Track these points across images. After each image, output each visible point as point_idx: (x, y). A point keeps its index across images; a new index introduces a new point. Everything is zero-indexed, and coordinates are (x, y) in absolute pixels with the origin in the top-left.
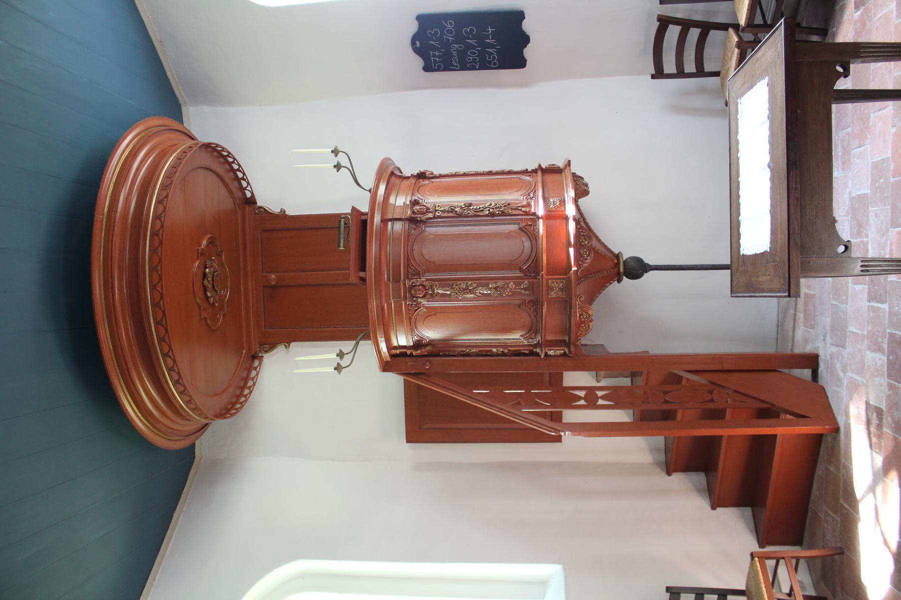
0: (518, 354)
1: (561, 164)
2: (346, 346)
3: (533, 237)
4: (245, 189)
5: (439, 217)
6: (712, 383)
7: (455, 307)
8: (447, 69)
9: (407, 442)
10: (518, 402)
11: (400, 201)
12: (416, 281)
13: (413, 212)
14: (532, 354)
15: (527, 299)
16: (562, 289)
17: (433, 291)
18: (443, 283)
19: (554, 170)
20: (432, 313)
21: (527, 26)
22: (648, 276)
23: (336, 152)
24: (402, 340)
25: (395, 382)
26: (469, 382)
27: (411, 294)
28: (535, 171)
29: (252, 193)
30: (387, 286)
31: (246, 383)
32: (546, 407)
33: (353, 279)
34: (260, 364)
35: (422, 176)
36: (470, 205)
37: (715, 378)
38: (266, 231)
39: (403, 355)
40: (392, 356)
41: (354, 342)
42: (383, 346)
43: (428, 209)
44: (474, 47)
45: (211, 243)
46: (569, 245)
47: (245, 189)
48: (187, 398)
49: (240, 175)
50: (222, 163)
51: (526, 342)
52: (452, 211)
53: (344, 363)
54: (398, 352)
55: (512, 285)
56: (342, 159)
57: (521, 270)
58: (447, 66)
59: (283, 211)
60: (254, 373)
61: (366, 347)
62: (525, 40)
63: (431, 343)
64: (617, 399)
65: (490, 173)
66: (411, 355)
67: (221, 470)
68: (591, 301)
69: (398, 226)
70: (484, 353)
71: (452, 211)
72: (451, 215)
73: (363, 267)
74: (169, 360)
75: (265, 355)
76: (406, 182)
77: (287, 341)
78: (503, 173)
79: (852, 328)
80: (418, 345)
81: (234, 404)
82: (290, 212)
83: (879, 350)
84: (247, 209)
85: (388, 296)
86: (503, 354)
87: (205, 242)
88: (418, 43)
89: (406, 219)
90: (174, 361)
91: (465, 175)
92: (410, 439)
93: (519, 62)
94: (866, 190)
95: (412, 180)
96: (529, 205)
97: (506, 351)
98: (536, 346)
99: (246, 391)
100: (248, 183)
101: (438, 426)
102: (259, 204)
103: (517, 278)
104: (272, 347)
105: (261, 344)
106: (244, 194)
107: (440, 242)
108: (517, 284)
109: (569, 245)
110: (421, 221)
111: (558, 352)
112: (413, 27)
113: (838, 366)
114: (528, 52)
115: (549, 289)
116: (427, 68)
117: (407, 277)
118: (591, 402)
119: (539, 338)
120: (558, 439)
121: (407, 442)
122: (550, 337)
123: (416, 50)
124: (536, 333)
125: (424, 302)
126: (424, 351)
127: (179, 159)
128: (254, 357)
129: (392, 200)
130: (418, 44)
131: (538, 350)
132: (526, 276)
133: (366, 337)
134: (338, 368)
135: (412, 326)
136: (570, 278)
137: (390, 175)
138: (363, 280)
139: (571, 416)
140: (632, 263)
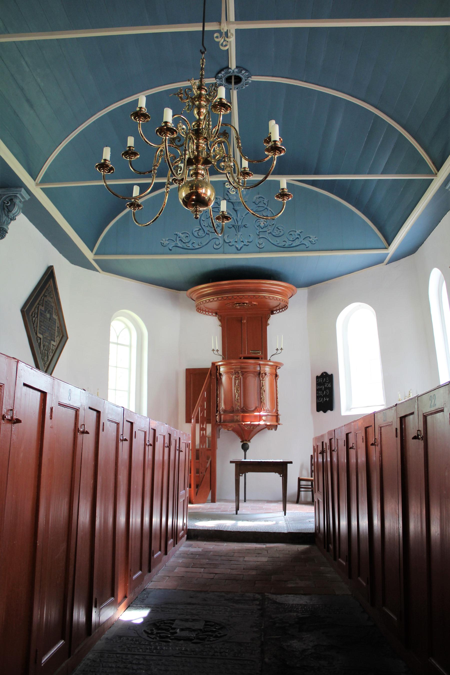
0: (217, 406)
1: (280, 422)
2: (220, 352)
3: (254, 411)
8: (317, 384)
9: (186, 369)
11: (267, 369)
12: (241, 374)
15: (234, 409)
16: (237, 420)
19: (277, 420)
20: (231, 379)
21: (329, 412)
23: (281, 349)
24: (222, 369)
25: (209, 366)
27: (236, 373)
28: (277, 413)
30: (239, 365)
33: (241, 355)
35: (276, 376)
37: (209, 469)
38: (262, 318)
39: (217, 370)
40: (217, 366)
41: (221, 354)
42: (220, 363)
44: (323, 393)
45: (255, 305)
46: (251, 422)
48: (204, 302)
49: (281, 310)
52: (263, 386)
53: (215, 352)
55: (239, 404)
57: (243, 407)
58: (318, 384)
60: (210, 314)
61: (220, 358)
63: (221, 379)
64: (203, 438)
65: (277, 398)
66: (217, 372)
69: (259, 369)
71: (263, 386)
73: (245, 358)
76: (274, 370)
77: (223, 326)
78: (277, 403)
80: (220, 374)
81: (200, 309)
82: (268, 327)
84: (270, 312)
85: (236, 365)
86: (217, 402)
87: (255, 303)
89: (260, 371)
90: (216, 301)
91: (276, 390)
92: (187, 369)
93: (318, 410)
95: (275, 373)
96: (264, 410)
98: (220, 412)
101: (192, 379)
102: (271, 316)
104: (220, 320)
105: (221, 316)
107: (252, 381)
109: (251, 422)
112: (329, 373)
114: (321, 412)
115: (237, 416)
116: (317, 377)
117: (242, 372)
118: (202, 429)
119: (222, 413)
120: (188, 420)
121: (186, 369)
122: (222, 416)
123: (322, 374)
124: (224, 412)
125: (234, 377)
128: (216, 313)
132: (241, 409)
133: (223, 359)
134: (213, 350)
135: (227, 373)
136: (240, 422)
137: (276, 366)
138: (241, 358)
139: (198, 426)
140: (247, 446)
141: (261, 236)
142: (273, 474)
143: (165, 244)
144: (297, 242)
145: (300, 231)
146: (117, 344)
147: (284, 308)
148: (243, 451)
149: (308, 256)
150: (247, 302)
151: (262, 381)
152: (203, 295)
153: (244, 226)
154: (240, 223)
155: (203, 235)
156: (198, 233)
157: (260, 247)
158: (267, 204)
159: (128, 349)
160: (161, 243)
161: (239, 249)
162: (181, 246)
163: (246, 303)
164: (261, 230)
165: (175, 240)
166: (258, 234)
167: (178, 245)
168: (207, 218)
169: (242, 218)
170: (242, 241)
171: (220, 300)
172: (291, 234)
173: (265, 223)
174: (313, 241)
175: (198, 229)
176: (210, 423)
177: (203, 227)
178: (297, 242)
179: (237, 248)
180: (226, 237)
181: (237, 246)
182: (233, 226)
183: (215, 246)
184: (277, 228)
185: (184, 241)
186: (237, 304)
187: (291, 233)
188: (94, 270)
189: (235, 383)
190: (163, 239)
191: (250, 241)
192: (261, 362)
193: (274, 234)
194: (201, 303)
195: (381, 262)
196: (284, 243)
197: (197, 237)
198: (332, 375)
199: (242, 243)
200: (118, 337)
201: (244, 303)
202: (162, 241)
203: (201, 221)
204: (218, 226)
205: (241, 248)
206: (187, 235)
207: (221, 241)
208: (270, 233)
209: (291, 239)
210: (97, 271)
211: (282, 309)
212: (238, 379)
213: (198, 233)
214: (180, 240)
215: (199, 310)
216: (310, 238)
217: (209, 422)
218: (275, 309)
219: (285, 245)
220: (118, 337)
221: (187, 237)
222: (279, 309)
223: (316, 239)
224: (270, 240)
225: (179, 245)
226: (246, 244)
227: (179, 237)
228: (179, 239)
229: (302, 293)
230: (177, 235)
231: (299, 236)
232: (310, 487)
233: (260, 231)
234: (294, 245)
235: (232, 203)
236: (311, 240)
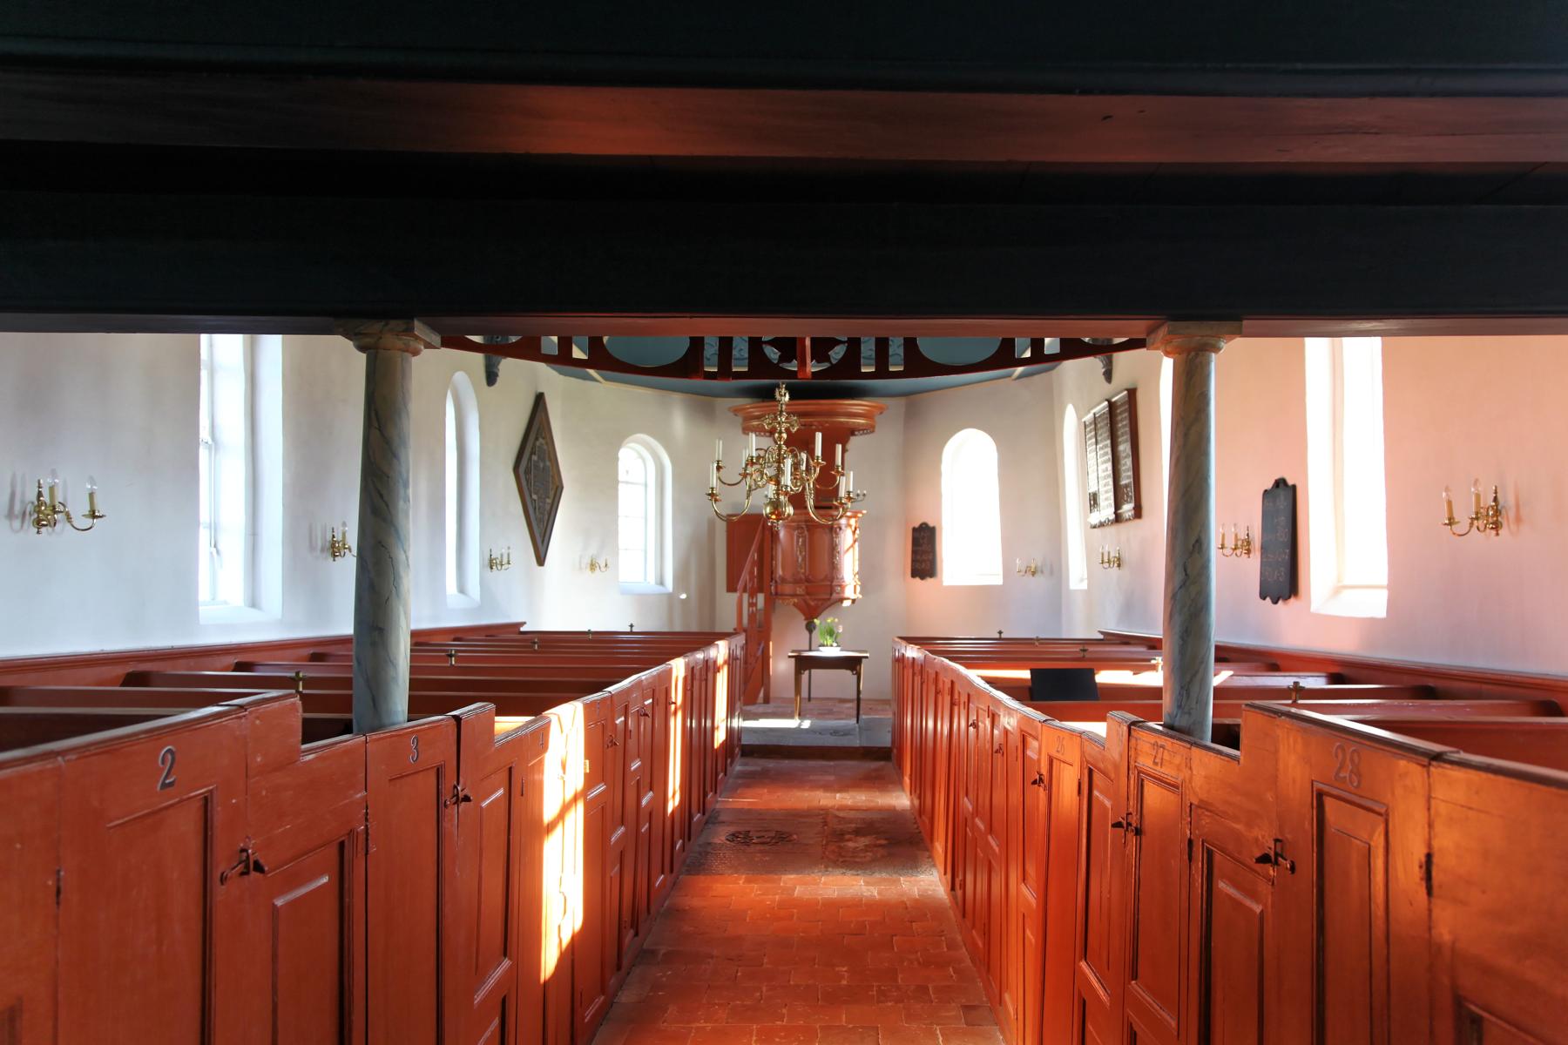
10: (751, 573)
27: (799, 527)
62: (922, 578)
64: (752, 616)
68: (795, 605)
93: (913, 576)
114: (917, 580)
116: (914, 530)
118: (752, 605)
120: (731, 588)
139: (746, 596)
142: (340, 338)
217: (761, 590)
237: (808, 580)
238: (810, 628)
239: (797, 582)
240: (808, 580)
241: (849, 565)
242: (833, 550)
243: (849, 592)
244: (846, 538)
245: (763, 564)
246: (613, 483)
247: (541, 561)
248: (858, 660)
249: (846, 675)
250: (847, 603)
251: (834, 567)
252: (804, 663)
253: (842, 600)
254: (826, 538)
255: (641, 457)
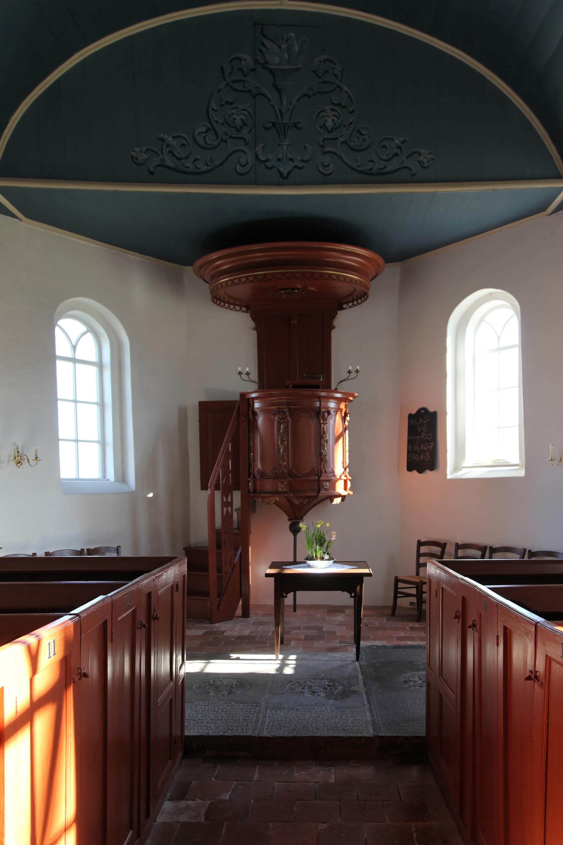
2: (254, 376)
4: (348, 305)
5: (321, 426)
6: (235, 565)
7: (274, 434)
13: (324, 412)
14: (250, 474)
17: (283, 423)
18: (286, 428)
21: (428, 473)
22: (291, 535)
24: (257, 405)
26: (235, 441)
27: (279, 412)
29: (345, 309)
31: (232, 304)
32: (222, 480)
34: (244, 312)
36: (327, 442)
39: (249, 406)
40: (249, 399)
41: (257, 380)
42: (254, 395)
43: (326, 420)
45: (313, 291)
47: (348, 305)
48: (224, 285)
49: (355, 303)
50: (359, 297)
51: (256, 471)
52: (324, 433)
54: (251, 402)
56: (353, 375)
57: (292, 468)
59: (334, 327)
60: (238, 308)
61: (255, 387)
62: (420, 471)
63: (255, 421)
64: (227, 518)
66: (249, 410)
67: (176, 284)
68: (276, 503)
70: (250, 449)
72: (322, 432)
73: (295, 387)
74: (245, 279)
75: (248, 315)
77: (257, 329)
79: (261, 627)
80: (255, 414)
81: (219, 300)
82: (334, 333)
83: (250, 633)
86: (249, 459)
87: (313, 289)
88: (423, 411)
89: (320, 408)
90: (244, 283)
93: (410, 469)
94: (324, 629)
97: (251, 460)
98: (254, 477)
99: (227, 305)
100: (350, 307)
103: (288, 468)
104: (254, 319)
106: (345, 304)
108: (285, 466)
110: (319, 417)
111: (250, 488)
112: (431, 410)
113: (243, 623)
114: (415, 473)
116: (411, 416)
117: (290, 410)
118: (226, 504)
119: (258, 477)
120: (204, 487)
122: (258, 483)
123: (419, 410)
125: (276, 418)
126: (251, 416)
127: (356, 281)
129: (333, 401)
130: (423, 411)
131: (252, 477)
133: (259, 387)
134: (240, 373)
135: (264, 410)
138: (288, 387)
139: (218, 495)
141: (327, 149)
143: (140, 160)
144: (394, 164)
145: (401, 139)
146: (74, 360)
147: (361, 298)
148: (291, 534)
149: (413, 193)
150: (299, 286)
151: (322, 425)
152: (222, 270)
153: (295, 125)
154: (286, 120)
155: (216, 143)
156: (205, 138)
157: (326, 172)
158: (339, 77)
159: (94, 370)
160: (132, 156)
161: (285, 175)
162: (173, 166)
163: (298, 289)
164: (327, 136)
165: (160, 153)
166: (321, 143)
167: (166, 163)
168: (222, 105)
169: (291, 107)
170: (291, 160)
171: (251, 282)
172: (384, 146)
173: (336, 119)
174: (425, 161)
175: (204, 129)
176: (237, 489)
177: (214, 124)
178: (394, 164)
179: (281, 173)
180: (259, 148)
181: (282, 169)
182: (274, 125)
183: (239, 168)
184: (359, 131)
185: (177, 155)
186: (281, 290)
187: (384, 143)
188: (6, 215)
189: (279, 429)
190: (136, 149)
191: (306, 158)
192: (323, 394)
193: (352, 144)
194: (219, 287)
195: (542, 208)
196: (370, 166)
197: (200, 146)
198: (435, 414)
199: (291, 163)
200: (499, 338)
201: (294, 289)
202: (133, 153)
203: (211, 111)
204: (244, 123)
205: (289, 173)
206: (184, 142)
207: (250, 158)
208: (345, 142)
209: (385, 157)
210: (15, 216)
211: (357, 300)
212: (284, 422)
213: (205, 138)
214: (170, 152)
215: (219, 299)
216: (420, 154)
217: (237, 487)
218: (345, 301)
219: (371, 169)
220: (499, 338)
221: (183, 145)
222: (353, 301)
223: (431, 156)
224: (345, 158)
225: (169, 163)
226: (299, 166)
227: (168, 146)
228: (168, 149)
229: (392, 272)
230: (163, 140)
231: (398, 151)
232: (399, 595)
233: (326, 137)
234: (389, 168)
235: (271, 71)
236: (421, 158)
237: (291, 475)
238: (295, 530)
239: (278, 476)
240: (291, 475)
241: (339, 458)
242: (320, 438)
243: (340, 488)
244: (336, 424)
245: (246, 454)
246: (47, 358)
247: (463, 598)
248: (359, 578)
249: (342, 598)
250: (337, 501)
251: (322, 460)
252: (286, 584)
253: (331, 498)
254: (313, 424)
255: (482, 320)
